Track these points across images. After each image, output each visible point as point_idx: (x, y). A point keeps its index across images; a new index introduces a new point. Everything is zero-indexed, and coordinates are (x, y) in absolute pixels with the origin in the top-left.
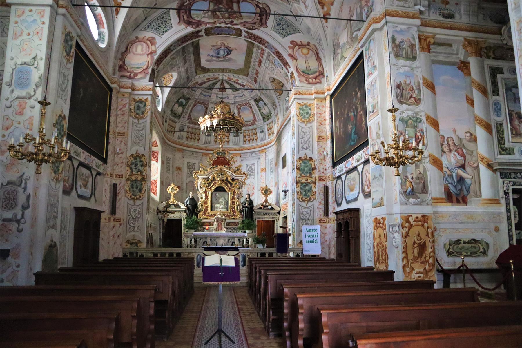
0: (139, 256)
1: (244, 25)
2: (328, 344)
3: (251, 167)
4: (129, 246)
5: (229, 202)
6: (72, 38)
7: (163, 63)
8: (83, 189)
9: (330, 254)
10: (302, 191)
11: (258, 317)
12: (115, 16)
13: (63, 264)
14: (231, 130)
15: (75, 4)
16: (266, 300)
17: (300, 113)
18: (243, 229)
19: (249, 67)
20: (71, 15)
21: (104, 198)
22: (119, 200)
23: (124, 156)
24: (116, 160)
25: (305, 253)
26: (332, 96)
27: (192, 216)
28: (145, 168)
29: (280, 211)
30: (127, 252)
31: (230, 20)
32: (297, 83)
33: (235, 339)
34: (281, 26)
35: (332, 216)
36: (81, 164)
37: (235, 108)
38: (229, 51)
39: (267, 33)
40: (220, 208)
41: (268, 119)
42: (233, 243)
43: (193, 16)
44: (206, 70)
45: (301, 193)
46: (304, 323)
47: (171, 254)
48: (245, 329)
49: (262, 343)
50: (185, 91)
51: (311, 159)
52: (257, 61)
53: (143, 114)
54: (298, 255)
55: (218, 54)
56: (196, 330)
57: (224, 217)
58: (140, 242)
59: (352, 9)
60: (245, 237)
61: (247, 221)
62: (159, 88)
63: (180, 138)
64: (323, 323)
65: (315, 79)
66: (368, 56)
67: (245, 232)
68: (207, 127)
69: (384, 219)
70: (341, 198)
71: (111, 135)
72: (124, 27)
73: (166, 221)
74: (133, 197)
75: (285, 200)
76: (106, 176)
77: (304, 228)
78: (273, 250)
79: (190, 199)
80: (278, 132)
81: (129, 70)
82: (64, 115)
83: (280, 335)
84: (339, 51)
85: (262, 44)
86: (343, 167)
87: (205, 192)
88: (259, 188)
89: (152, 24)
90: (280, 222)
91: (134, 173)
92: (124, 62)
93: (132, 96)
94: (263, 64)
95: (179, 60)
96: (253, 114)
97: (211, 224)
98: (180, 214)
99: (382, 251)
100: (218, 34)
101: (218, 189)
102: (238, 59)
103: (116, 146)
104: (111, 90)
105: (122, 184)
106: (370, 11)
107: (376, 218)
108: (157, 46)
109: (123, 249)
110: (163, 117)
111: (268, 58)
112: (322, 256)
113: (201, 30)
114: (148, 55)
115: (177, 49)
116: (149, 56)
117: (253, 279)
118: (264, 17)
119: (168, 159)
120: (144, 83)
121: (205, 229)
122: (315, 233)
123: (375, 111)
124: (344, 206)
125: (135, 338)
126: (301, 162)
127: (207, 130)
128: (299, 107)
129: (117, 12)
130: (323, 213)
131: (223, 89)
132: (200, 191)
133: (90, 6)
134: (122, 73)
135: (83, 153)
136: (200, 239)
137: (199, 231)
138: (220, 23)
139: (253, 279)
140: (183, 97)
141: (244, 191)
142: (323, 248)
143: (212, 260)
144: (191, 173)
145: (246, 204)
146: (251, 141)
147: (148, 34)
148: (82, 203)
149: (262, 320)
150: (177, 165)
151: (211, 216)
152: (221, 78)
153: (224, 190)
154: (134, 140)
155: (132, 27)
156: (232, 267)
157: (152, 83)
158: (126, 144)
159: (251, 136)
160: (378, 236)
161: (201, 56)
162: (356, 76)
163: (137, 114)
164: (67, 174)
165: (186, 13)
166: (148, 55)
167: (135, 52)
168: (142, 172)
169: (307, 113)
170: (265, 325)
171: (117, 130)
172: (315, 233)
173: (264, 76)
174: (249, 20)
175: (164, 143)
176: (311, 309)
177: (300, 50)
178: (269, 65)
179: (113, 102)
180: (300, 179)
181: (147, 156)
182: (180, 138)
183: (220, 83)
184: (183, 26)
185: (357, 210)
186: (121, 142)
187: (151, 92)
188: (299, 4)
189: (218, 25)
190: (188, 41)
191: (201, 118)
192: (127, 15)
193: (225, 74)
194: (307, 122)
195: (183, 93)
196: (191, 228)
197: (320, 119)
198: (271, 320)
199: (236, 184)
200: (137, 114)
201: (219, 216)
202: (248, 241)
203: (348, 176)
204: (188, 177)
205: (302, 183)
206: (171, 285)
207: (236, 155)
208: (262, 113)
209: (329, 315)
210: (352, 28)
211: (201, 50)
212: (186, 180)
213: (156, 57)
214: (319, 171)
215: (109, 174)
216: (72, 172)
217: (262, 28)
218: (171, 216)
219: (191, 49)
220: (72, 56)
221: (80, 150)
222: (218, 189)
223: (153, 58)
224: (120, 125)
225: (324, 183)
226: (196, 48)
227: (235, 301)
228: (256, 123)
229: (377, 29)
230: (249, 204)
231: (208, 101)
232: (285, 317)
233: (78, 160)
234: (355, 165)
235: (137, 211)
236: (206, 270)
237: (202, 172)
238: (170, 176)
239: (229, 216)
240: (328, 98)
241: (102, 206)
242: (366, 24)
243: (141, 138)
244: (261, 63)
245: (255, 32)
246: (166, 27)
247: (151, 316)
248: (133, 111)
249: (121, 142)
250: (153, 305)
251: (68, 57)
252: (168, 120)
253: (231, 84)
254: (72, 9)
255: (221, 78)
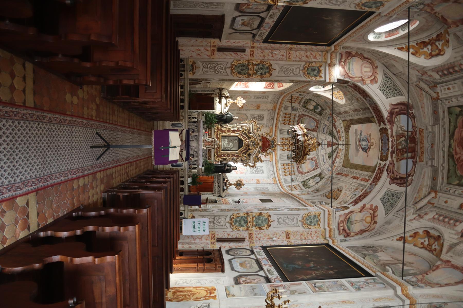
0: (182, 72)
1: (391, 164)
2: (83, 262)
3: (261, 170)
4: (191, 64)
5: (229, 152)
6: (378, 8)
7: (354, 91)
8: (241, 22)
9: (183, 243)
10: (240, 218)
11: (124, 181)
12: (396, 47)
13: (174, 5)
14: (294, 152)
15: (410, 10)
16: (139, 188)
17: (311, 215)
18: (206, 164)
19: (352, 168)
20: (400, 6)
21: (232, 41)
22: (231, 55)
23: (270, 58)
24: (267, 51)
25: (184, 221)
26: (328, 245)
27: (217, 119)
28: (259, 77)
29: (221, 197)
30: (185, 62)
31: (395, 151)
32: (339, 213)
33: (101, 160)
34: (392, 197)
35: (217, 246)
36: (263, 20)
37: (314, 156)
38: (366, 150)
39: (385, 185)
40: (224, 143)
41: (303, 185)
42: (193, 156)
43: (398, 117)
44: (347, 129)
45: (238, 217)
46: (110, 232)
47: (183, 101)
48: (111, 169)
49: (97, 186)
50: (328, 111)
51: (269, 226)
52: (358, 176)
53: (308, 74)
54: (181, 214)
55: (363, 140)
56: (112, 124)
57: (216, 147)
58: (194, 73)
59: (412, 265)
60: (198, 166)
61: (212, 167)
62: (331, 87)
63: (286, 107)
64: (105, 257)
65: (343, 229)
66: (369, 281)
67: (203, 166)
68: (296, 131)
69: (215, 297)
70: (234, 254)
71: (288, 46)
72: (387, 55)
73: (213, 96)
74: (234, 67)
75: (231, 202)
76: (252, 43)
77: (207, 220)
78: (187, 192)
79: (232, 117)
80: (292, 195)
81: (347, 61)
82: (308, 3)
83: (106, 204)
84: (370, 252)
85: (374, 180)
86: (262, 256)
87: (238, 130)
88: (242, 178)
89: (390, 80)
90: (211, 197)
91: (255, 67)
92: (354, 56)
93: (324, 64)
94: (354, 180)
95: (356, 105)
96: (308, 172)
97: (210, 136)
98: (220, 107)
99: (185, 295)
100: (382, 140)
101: (240, 142)
102: (358, 158)
103: (278, 51)
104: (330, 45)
105: (245, 56)
106: (414, 284)
107: (215, 290)
108: (370, 85)
109: (188, 59)
110: (303, 93)
111: (361, 185)
112: (181, 236)
113: (385, 125)
114: (361, 77)
115: (367, 104)
116: (360, 78)
117: (159, 176)
118: (399, 182)
119: (267, 97)
120: (337, 72)
121: (206, 131)
122: (202, 230)
123: (317, 289)
124: (226, 258)
125: (97, 65)
126: (266, 217)
127: (293, 131)
128: (317, 214)
129: (401, 49)
130: (220, 237)
131: (331, 144)
132: (239, 126)
133: (408, 22)
134: (344, 55)
135: (273, 21)
136: (196, 126)
137: (204, 125)
138: (392, 141)
139: (159, 176)
140: (322, 110)
141: (239, 165)
142: (188, 237)
143: (175, 139)
144: (255, 118)
145: (228, 166)
146: (284, 170)
147: (380, 77)
148: (228, 21)
149: (121, 185)
150: (261, 105)
151: (217, 134)
152: (340, 142)
153: (239, 148)
154: (285, 67)
155: (386, 63)
156: (168, 158)
157: (336, 81)
158: (280, 60)
159: (288, 170)
160: (198, 291)
161: (360, 125)
162: (348, 270)
163: (308, 69)
164: (254, 7)
165: (400, 111)
166: (361, 77)
167: (363, 66)
168: (256, 74)
169: (311, 222)
170: (116, 188)
171: (292, 52)
172: (202, 230)
173: (343, 182)
174: (396, 168)
175: (281, 93)
176: (124, 238)
177: (370, 215)
178: (354, 186)
179: (319, 47)
180: (251, 216)
181: (270, 78)
182: (286, 107)
183: (336, 142)
184: (389, 108)
185: (223, 271)
186: (283, 56)
187: (328, 81)
188: (413, 214)
189: (390, 140)
190: (374, 112)
191: (304, 125)
192: (398, 57)
193: (344, 147)
194: (303, 222)
195: (326, 109)
196: (206, 118)
197: (306, 234)
198: (120, 194)
199: (246, 157)
200: (308, 69)
201: (217, 142)
202: (195, 168)
203: (254, 261)
204: (252, 115)
205: (247, 218)
206: (152, 100)
207: (272, 158)
208: (309, 180)
209: (112, 264)
210: (394, 265)
211: (366, 124)
212: (249, 113)
213: (359, 84)
214: (258, 234)
215: (254, 45)
216: (256, 12)
217: (388, 180)
218: (217, 101)
219: (367, 116)
220: (361, 8)
221: (275, 18)
222: (240, 142)
223: (358, 82)
224: (298, 54)
225: (247, 238)
226: (368, 120)
227: (140, 158)
228: (300, 175)
229: (396, 292)
230: (227, 169)
231: (319, 132)
232: (119, 210)
233: (266, 17)
234: (265, 268)
235: (221, 70)
236: (165, 133)
237: (256, 127)
238: (252, 99)
239: (217, 152)
240: (325, 242)
241: (225, 39)
242: (400, 279)
243: (286, 73)
244: (355, 179)
245: (385, 173)
246: (387, 92)
247: (121, 81)
248: (311, 65)
249: (283, 56)
250: (132, 82)
251: (360, 5)
252: (301, 96)
253: (335, 152)
254: (405, 7)
255: (340, 142)
